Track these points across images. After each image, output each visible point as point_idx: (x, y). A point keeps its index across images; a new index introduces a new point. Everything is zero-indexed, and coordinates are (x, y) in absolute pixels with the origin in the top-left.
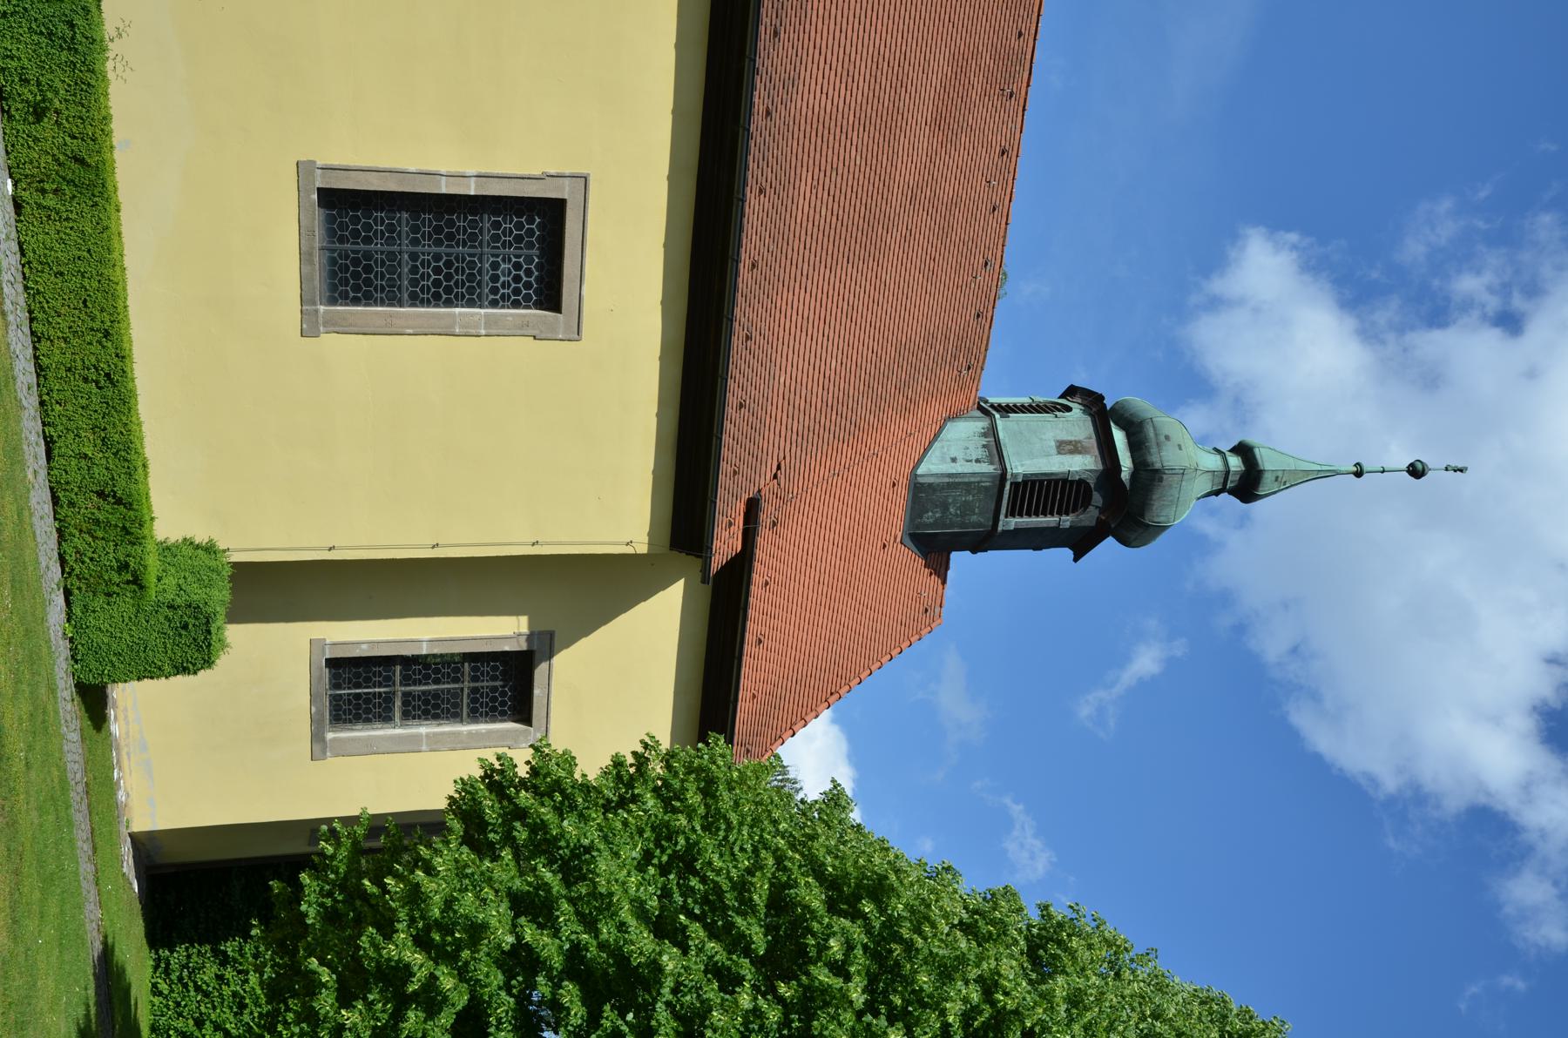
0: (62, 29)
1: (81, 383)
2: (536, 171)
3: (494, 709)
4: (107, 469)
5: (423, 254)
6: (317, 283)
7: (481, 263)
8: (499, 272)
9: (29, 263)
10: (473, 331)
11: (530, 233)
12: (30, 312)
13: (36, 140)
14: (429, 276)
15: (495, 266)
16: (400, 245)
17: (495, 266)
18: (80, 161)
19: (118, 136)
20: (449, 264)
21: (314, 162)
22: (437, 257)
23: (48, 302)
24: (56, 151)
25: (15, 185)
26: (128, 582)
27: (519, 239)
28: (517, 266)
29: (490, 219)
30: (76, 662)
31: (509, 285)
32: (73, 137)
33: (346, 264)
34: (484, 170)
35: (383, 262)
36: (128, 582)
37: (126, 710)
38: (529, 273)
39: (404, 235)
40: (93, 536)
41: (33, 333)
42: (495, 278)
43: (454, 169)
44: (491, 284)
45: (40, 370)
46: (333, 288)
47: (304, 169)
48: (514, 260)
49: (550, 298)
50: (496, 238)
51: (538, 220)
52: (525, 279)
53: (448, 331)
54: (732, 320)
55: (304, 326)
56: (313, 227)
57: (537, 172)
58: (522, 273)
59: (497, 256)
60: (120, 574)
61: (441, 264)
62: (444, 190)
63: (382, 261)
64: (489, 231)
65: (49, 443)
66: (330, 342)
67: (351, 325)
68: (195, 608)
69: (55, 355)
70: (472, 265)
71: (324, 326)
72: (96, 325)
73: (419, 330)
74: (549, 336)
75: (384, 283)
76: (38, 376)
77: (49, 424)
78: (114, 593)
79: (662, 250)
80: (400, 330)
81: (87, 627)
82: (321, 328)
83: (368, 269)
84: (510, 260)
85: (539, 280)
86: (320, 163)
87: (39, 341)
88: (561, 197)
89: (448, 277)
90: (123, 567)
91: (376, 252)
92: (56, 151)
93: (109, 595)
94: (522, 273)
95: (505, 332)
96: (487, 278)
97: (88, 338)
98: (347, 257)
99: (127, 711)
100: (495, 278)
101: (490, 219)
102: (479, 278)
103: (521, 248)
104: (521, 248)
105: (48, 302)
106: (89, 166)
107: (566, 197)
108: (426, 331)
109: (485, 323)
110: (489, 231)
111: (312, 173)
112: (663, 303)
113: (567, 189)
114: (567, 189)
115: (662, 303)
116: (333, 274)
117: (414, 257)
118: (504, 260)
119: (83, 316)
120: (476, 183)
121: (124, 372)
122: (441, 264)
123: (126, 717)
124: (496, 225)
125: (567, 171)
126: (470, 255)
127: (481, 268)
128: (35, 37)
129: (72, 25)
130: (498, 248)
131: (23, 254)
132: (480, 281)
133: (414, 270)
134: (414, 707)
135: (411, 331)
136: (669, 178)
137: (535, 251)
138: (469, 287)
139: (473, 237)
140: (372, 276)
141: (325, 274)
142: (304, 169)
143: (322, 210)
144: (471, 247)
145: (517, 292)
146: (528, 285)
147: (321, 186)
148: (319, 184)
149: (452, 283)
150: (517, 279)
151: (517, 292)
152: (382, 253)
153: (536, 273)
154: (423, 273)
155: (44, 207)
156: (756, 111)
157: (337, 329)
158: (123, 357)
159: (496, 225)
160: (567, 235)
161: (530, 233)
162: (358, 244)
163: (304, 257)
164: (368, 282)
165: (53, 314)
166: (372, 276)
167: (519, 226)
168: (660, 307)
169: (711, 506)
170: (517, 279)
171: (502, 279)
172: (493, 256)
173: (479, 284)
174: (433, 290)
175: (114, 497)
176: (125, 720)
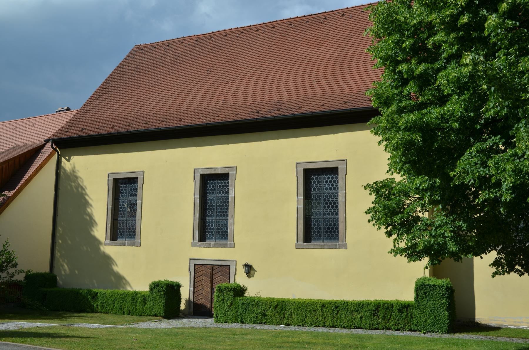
0: (244, 306)
1: (338, 315)
2: (193, 183)
3: (227, 186)
4: (365, 312)
5: (323, 211)
6: (330, 244)
7: (326, 193)
8: (329, 187)
9: (303, 325)
10: (344, 195)
11: (316, 178)
12: (316, 326)
13: (271, 317)
14: (330, 209)
15: (327, 189)
16: (321, 219)
17: (327, 189)
18: (276, 306)
19: (272, 296)
20: (327, 203)
21: (296, 244)
22: (325, 207)
23: (314, 321)
24: (274, 312)
25: (282, 324)
26: (407, 310)
27: (318, 182)
28: (327, 182)
29: (313, 191)
30: (438, 331)
31: (333, 184)
32: (270, 307)
33: (327, 235)
34: (296, 194)
35: (327, 224)
36: (407, 310)
37: (515, 322)
38: (329, 178)
39: (318, 217)
40: (390, 319)
41: (323, 327)
42: (330, 189)
43: (296, 203)
44: (332, 190)
45: (334, 326)
46: (335, 239)
47: (298, 247)
48: (325, 183)
49: (334, 171)
50: (318, 189)
51: (313, 177)
52: (330, 179)
53: (344, 202)
54: (312, 113)
55: (344, 248)
56: (313, 245)
57: (296, 178)
58: (329, 180)
59: (323, 188)
60: (404, 312)
61: (326, 206)
62: (302, 206)
63: (326, 224)
64: (316, 191)
65: (356, 328)
66: (348, 240)
67: (343, 234)
68: (418, 289)
69: (329, 322)
70: (327, 196)
71: (344, 242)
72: (320, 309)
73: (344, 212)
74: (345, 170)
75: (333, 223)
76: (336, 327)
77: (351, 327)
78: (410, 315)
79: (318, 137)
80: (344, 218)
81: (424, 326)
82: (344, 243)
83: (329, 228)
84: (325, 184)
85: (330, 175)
86: (296, 242)
87: (325, 325)
88: (303, 171)
89: (330, 203)
90: (400, 310)
91: (323, 226)
92: (274, 312)
93: (412, 317)
94: (329, 180)
95: (344, 184)
96: (330, 191)
97: (324, 312)
98: (325, 235)
99: (516, 322)
100: (330, 189)
101: (313, 191)
102: (331, 194)
103: (321, 181)
104: (321, 181)
105: (314, 321)
106: (277, 304)
107: (303, 169)
108: (344, 210)
109: (342, 191)
110: (316, 191)
111: (299, 244)
112: (334, 134)
113: (300, 169)
114: (300, 169)
115: (334, 134)
116: (331, 239)
117: (324, 214)
118: (325, 186)
119: (318, 312)
120: (300, 197)
121: (335, 303)
122: (326, 206)
123: (519, 322)
124: (314, 189)
125: (295, 169)
126: (323, 197)
127: (327, 193)
128: (246, 313)
129: (243, 304)
130: (321, 188)
131: (300, 326)
132: (335, 193)
133: (329, 214)
134: (318, 209)
135: (345, 215)
136: (296, 138)
137: (322, 177)
138: (333, 197)
139: (318, 196)
140: (331, 227)
141: (331, 241)
142: (298, 247)
143: (312, 242)
144: (321, 197)
145: (334, 182)
146: (332, 178)
147: (302, 242)
148: (302, 243)
149: (332, 202)
150: (330, 182)
151: (334, 182)
152: (323, 224)
153: (316, 176)
154: (329, 211)
155: (288, 318)
156: (310, 111)
157: (344, 238)
158: (331, 302)
159: (314, 189)
160: (314, 167)
161: (316, 178)
162: (321, 231)
163: (322, 247)
164: (333, 228)
165: (317, 320)
166: (331, 227)
167: (122, 190)
168: (336, 135)
169: (352, 110)
170: (330, 182)
171: (331, 186)
172: (323, 190)
173: (333, 193)
174: (335, 208)
175: (375, 311)
176: (520, 323)
